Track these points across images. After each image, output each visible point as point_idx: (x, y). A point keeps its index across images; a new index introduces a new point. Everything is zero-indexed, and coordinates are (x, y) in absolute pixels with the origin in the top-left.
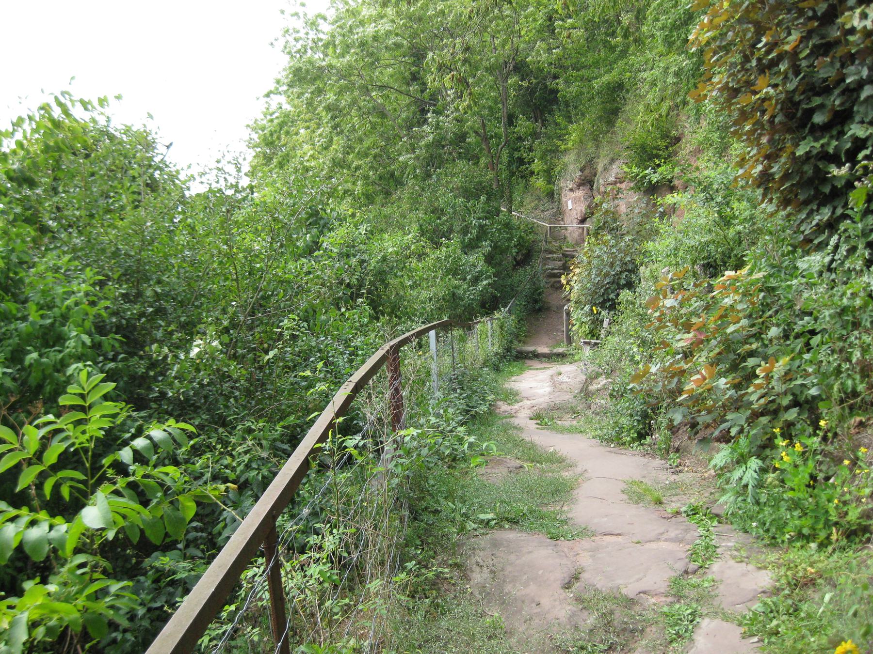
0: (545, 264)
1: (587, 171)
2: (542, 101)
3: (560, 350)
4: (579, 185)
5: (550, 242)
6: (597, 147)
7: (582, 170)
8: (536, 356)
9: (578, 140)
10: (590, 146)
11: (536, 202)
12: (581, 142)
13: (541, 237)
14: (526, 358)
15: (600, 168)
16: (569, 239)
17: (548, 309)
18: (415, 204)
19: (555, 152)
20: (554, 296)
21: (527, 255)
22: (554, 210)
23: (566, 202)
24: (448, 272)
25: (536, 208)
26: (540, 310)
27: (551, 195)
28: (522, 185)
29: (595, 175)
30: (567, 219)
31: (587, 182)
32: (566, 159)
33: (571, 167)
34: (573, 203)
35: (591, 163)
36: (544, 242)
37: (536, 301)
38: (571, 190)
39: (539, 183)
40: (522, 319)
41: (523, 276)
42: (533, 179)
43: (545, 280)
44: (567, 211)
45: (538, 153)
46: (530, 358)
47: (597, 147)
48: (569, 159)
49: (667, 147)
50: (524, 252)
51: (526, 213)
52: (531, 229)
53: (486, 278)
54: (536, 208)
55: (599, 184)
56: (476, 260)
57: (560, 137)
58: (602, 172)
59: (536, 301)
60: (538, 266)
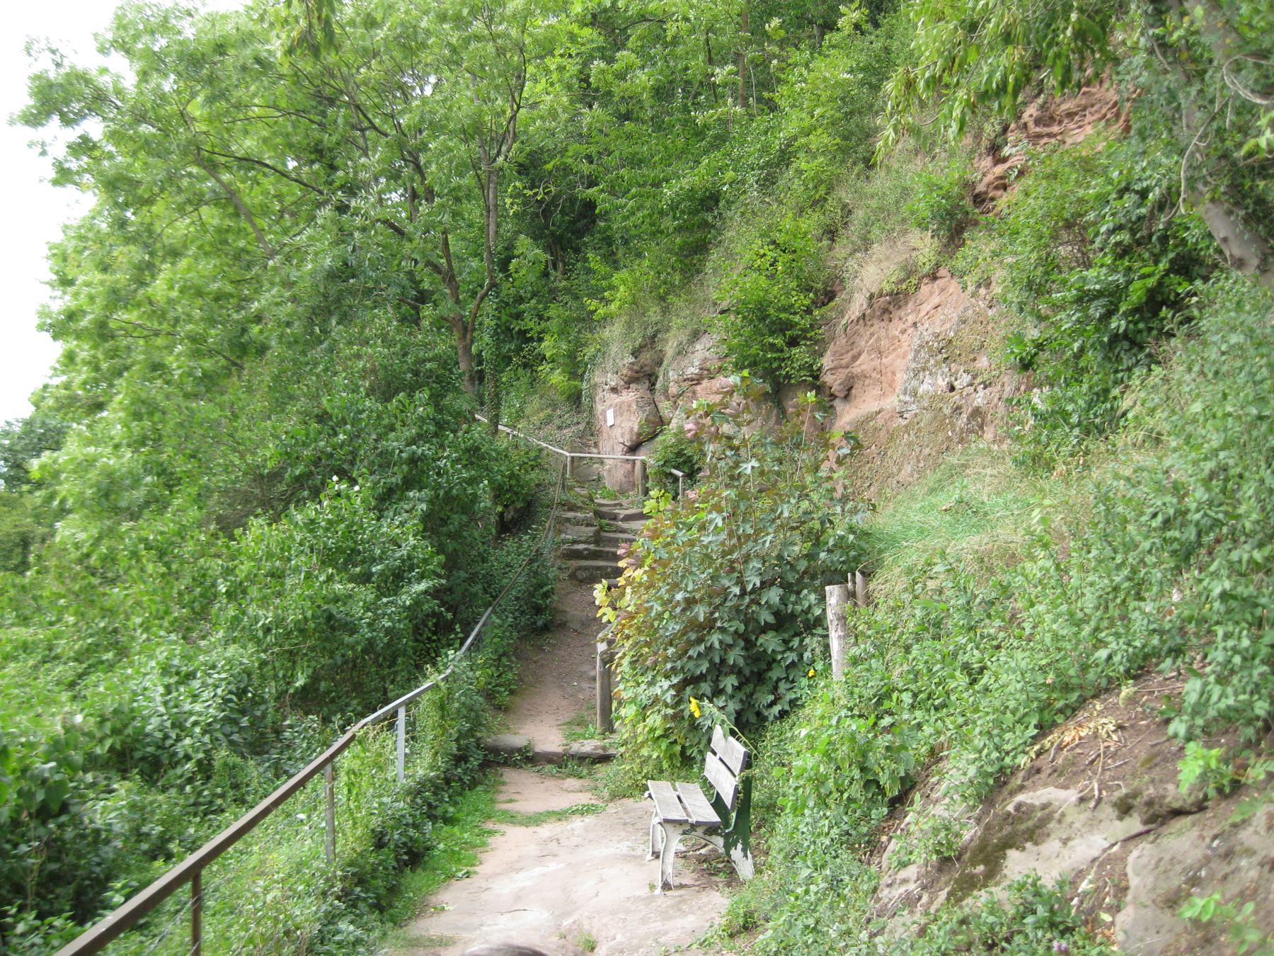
0: (560, 532)
1: (646, 357)
2: (570, 227)
3: (588, 746)
4: (630, 381)
5: (571, 488)
6: (665, 311)
7: (635, 353)
8: (529, 759)
9: (630, 299)
10: (654, 313)
11: (549, 411)
12: (634, 302)
13: (554, 477)
14: (506, 763)
15: (670, 349)
16: (607, 482)
17: (563, 626)
18: (281, 400)
19: (588, 321)
20: (577, 597)
21: (520, 511)
22: (581, 427)
23: (604, 412)
24: (328, 558)
25: (548, 421)
26: (546, 628)
27: (575, 399)
28: (524, 380)
29: (660, 363)
30: (605, 445)
31: (645, 377)
32: (606, 334)
33: (614, 349)
34: (617, 415)
35: (652, 341)
36: (558, 489)
37: (538, 610)
38: (614, 390)
39: (557, 378)
40: (504, 654)
41: (511, 557)
42: (544, 368)
43: (559, 562)
44: (605, 429)
45: (554, 325)
46: (515, 765)
47: (665, 311)
48: (613, 332)
49: (808, 311)
50: (519, 505)
51: (523, 428)
52: (536, 461)
53: (422, 577)
54: (548, 421)
55: (667, 380)
56: (402, 532)
57: (596, 293)
58: (674, 358)
59: (538, 610)
60: (546, 539)
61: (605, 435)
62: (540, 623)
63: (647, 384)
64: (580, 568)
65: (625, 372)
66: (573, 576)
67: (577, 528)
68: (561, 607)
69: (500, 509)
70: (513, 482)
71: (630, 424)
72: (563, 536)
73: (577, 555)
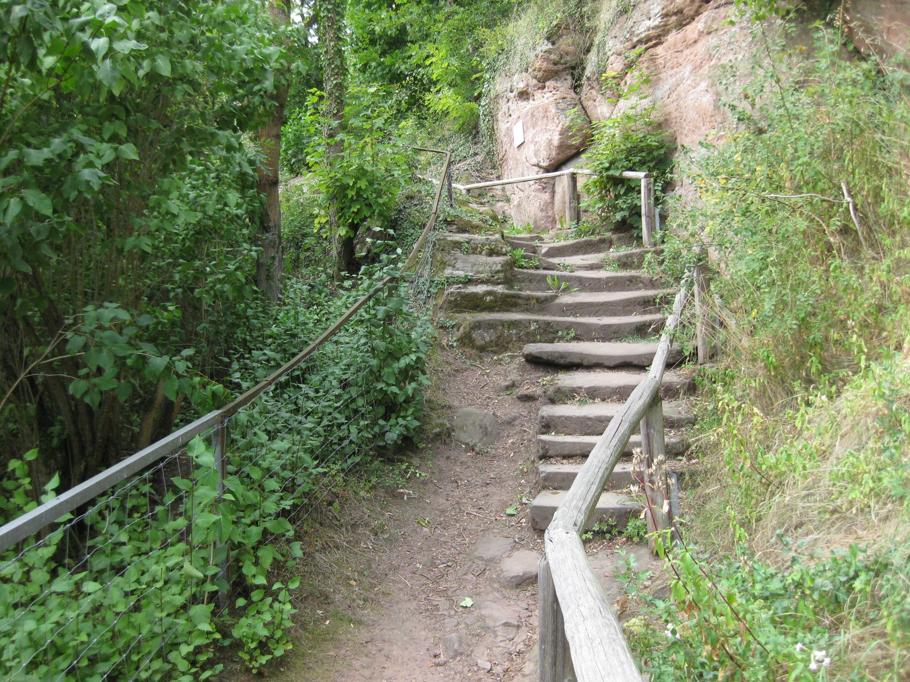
0: (444, 264)
1: (566, 43)
4: (542, 81)
17: (445, 436)
22: (479, 159)
23: (509, 130)
26: (408, 445)
34: (528, 128)
37: (391, 407)
59: (391, 407)
61: (511, 163)
62: (392, 436)
63: (569, 81)
64: (477, 326)
65: (537, 65)
66: (466, 340)
67: (473, 258)
68: (441, 398)
69: (342, 231)
70: (363, 184)
71: (547, 136)
72: (448, 272)
73: (474, 303)
